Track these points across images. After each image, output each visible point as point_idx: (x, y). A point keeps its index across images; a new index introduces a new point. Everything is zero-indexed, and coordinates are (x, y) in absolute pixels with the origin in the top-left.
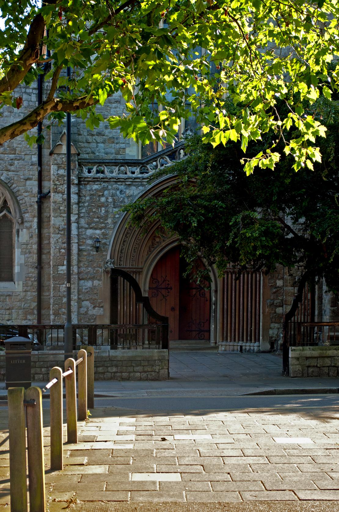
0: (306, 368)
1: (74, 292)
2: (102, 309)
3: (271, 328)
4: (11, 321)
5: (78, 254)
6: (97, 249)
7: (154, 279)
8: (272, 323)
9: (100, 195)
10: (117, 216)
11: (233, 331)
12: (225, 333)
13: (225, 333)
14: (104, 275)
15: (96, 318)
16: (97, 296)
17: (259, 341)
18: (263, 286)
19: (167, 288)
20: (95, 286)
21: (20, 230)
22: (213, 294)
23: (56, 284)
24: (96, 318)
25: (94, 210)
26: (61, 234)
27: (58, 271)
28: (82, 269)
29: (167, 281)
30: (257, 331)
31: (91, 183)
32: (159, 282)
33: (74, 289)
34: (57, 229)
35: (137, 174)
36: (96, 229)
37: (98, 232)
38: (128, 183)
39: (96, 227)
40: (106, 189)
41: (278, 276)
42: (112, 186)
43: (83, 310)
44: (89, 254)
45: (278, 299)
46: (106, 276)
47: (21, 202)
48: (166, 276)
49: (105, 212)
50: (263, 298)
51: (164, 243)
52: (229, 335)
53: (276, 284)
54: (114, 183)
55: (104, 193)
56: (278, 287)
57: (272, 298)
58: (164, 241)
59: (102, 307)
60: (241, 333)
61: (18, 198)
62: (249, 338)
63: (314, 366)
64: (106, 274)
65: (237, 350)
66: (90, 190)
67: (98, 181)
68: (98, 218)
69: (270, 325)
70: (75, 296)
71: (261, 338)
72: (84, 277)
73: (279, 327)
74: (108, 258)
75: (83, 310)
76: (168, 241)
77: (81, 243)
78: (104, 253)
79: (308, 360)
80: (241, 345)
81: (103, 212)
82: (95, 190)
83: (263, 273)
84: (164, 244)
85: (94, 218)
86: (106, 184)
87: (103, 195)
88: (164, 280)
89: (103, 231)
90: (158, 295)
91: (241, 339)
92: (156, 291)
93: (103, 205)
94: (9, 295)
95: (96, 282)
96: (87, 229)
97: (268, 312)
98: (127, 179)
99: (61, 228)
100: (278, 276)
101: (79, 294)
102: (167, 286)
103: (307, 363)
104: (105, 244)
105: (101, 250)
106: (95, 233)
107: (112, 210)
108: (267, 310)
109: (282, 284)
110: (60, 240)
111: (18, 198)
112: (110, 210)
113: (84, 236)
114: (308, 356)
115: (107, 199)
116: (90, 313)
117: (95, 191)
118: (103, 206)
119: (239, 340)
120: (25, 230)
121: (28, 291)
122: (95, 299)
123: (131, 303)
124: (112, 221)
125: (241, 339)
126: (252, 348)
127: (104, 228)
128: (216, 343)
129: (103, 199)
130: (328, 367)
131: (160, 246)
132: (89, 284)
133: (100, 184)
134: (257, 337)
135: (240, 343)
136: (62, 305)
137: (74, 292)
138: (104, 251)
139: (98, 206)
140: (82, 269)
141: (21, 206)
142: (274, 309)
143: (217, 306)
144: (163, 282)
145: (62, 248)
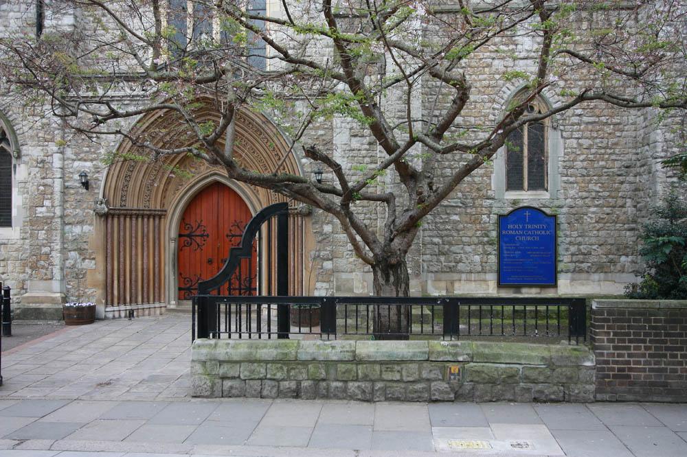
0: (220, 381)
1: (55, 240)
2: (93, 262)
4: (5, 275)
5: (63, 193)
6: (86, 185)
7: (187, 224)
8: (318, 281)
14: (96, 220)
15: (86, 272)
19: (202, 236)
20: (85, 233)
21: (17, 166)
23: (33, 230)
24: (86, 272)
26: (40, 167)
27: (36, 213)
28: (68, 211)
32: (192, 228)
33: (56, 236)
34: (35, 160)
35: (138, 91)
36: (85, 160)
37: (88, 164)
38: (126, 102)
39: (85, 158)
43: (69, 263)
44: (77, 193)
45: (326, 250)
47: (18, 132)
56: (325, 234)
59: (94, 259)
61: (15, 128)
63: (233, 378)
70: (57, 245)
72: (71, 221)
73: (328, 287)
74: (101, 197)
75: (69, 263)
76: (197, 177)
77: (67, 179)
78: (96, 191)
79: (222, 367)
84: (193, 181)
89: (94, 162)
90: (191, 244)
94: (5, 244)
95: (86, 228)
96: (74, 160)
98: (123, 96)
99: (39, 160)
101: (63, 243)
103: (222, 371)
105: (93, 187)
109: (331, 231)
110: (38, 175)
111: (15, 128)
113: (71, 170)
114: (222, 359)
116: (79, 266)
120: (22, 166)
121: (26, 239)
122: (85, 249)
130: (261, 379)
131: (189, 183)
132: (77, 230)
136: (41, 257)
137: (55, 240)
138: (96, 188)
140: (68, 211)
141: (18, 137)
144: (198, 228)
145: (40, 185)
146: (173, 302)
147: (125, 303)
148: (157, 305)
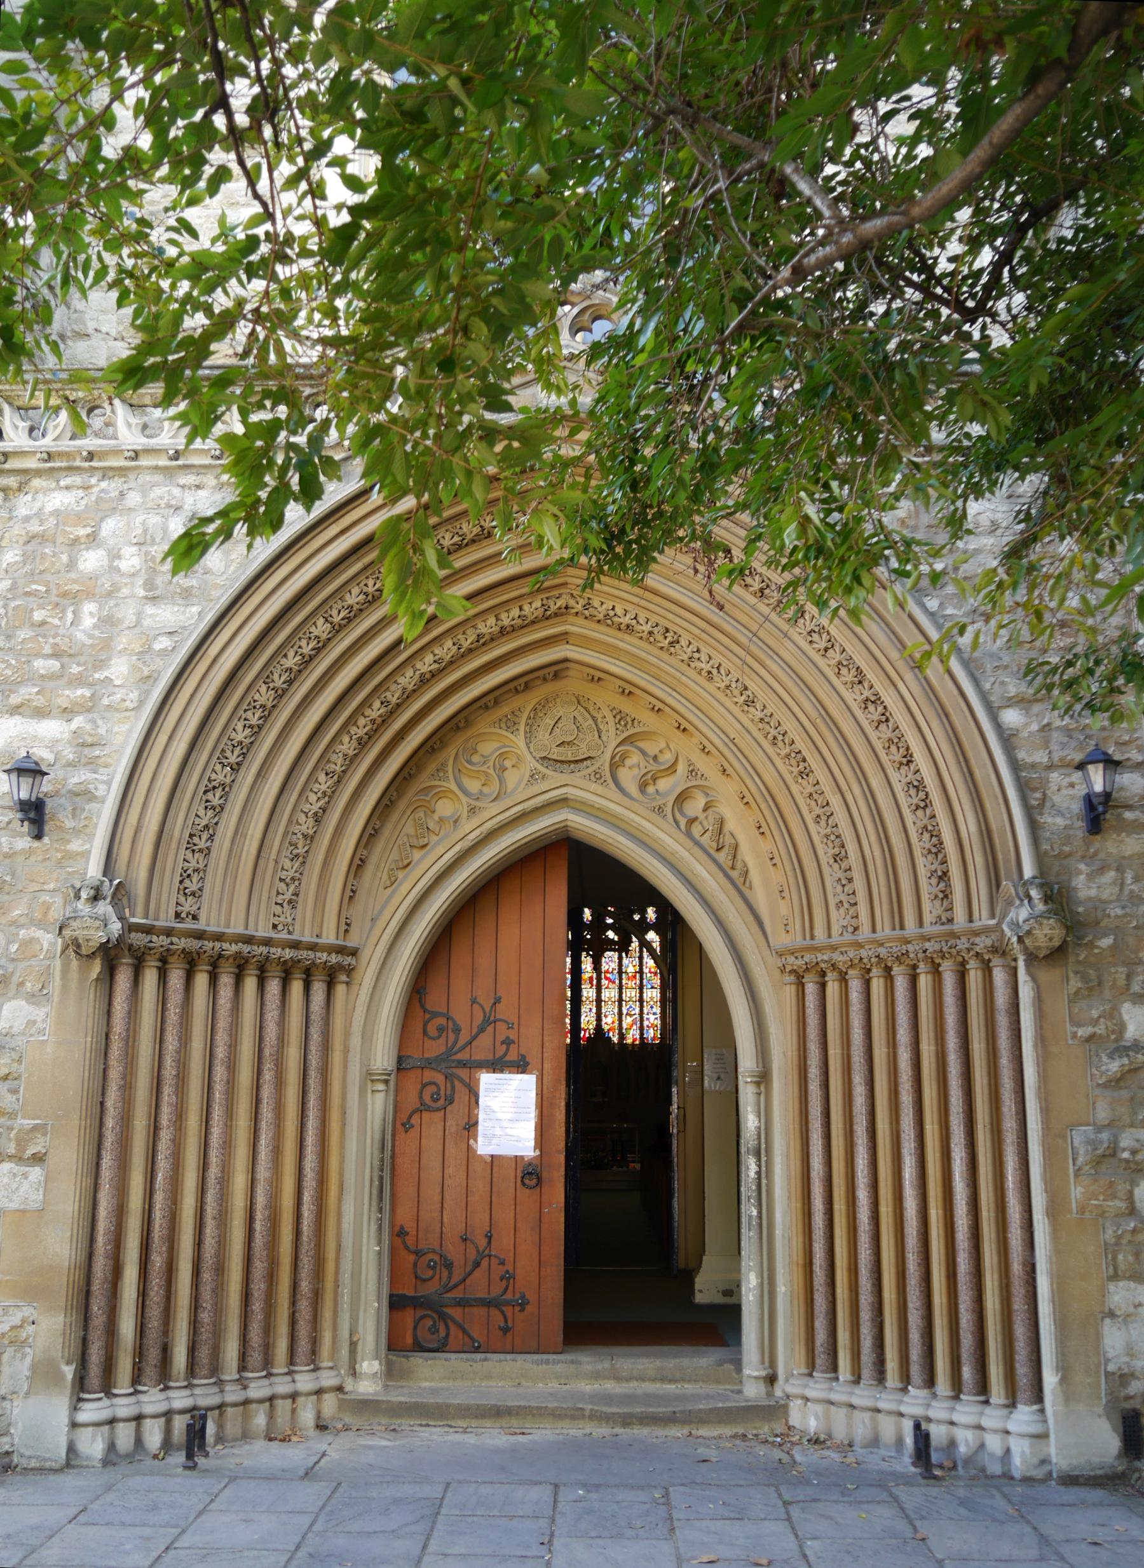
3: (1111, 1314)
8: (1115, 1277)
9: (76, 541)
10: (163, 643)
11: (865, 1315)
12: (820, 1324)
13: (820, 1324)
16: (15, 1091)
17: (1038, 1396)
18: (1041, 1040)
22: (747, 1094)
25: (38, 616)
29: (501, 1026)
30: (1020, 1331)
31: (36, 482)
32: (457, 1030)
36: (41, 713)
37: (52, 728)
39: (40, 701)
40: (115, 506)
41: (1129, 977)
42: (144, 494)
46: (74, 974)
48: (497, 1001)
49: (95, 626)
50: (1046, 1111)
51: (475, 822)
52: (843, 1337)
53: (1122, 1027)
54: (158, 478)
55: (97, 527)
57: (1102, 1114)
58: (473, 810)
59: (38, 1159)
60: (915, 1336)
62: (967, 1372)
64: (75, 963)
65: (900, 1441)
66: (27, 519)
67: (71, 469)
68: (56, 655)
69: (1103, 1293)
71: (1050, 1379)
78: (75, 846)
80: (918, 1411)
81: (88, 622)
82: (56, 513)
83: (1032, 958)
85: (39, 655)
86: (111, 486)
87: (93, 539)
88: (489, 1021)
89: (78, 721)
90: (450, 1101)
91: (915, 1370)
92: (439, 1078)
93: (87, 590)
97: (1082, 1210)
100: (1129, 977)
102: (499, 1054)
104: (85, 794)
105: (61, 829)
106: (35, 737)
107: (139, 615)
108: (1076, 1192)
112: (128, 613)
115: (115, 555)
117: (53, 521)
118: (90, 595)
119: (906, 1378)
123: (264, 1141)
124: (134, 668)
125: (915, 1370)
126: (994, 1443)
127: (88, 707)
128: (771, 1379)
129: (91, 560)
133: (87, 488)
134: (1022, 1370)
135: (915, 1402)
138: (76, 832)
139: (64, 595)
142: (1122, 1188)
143: (769, 1163)
146: (370, 1366)
147: (164, 1377)
148: (305, 1382)
